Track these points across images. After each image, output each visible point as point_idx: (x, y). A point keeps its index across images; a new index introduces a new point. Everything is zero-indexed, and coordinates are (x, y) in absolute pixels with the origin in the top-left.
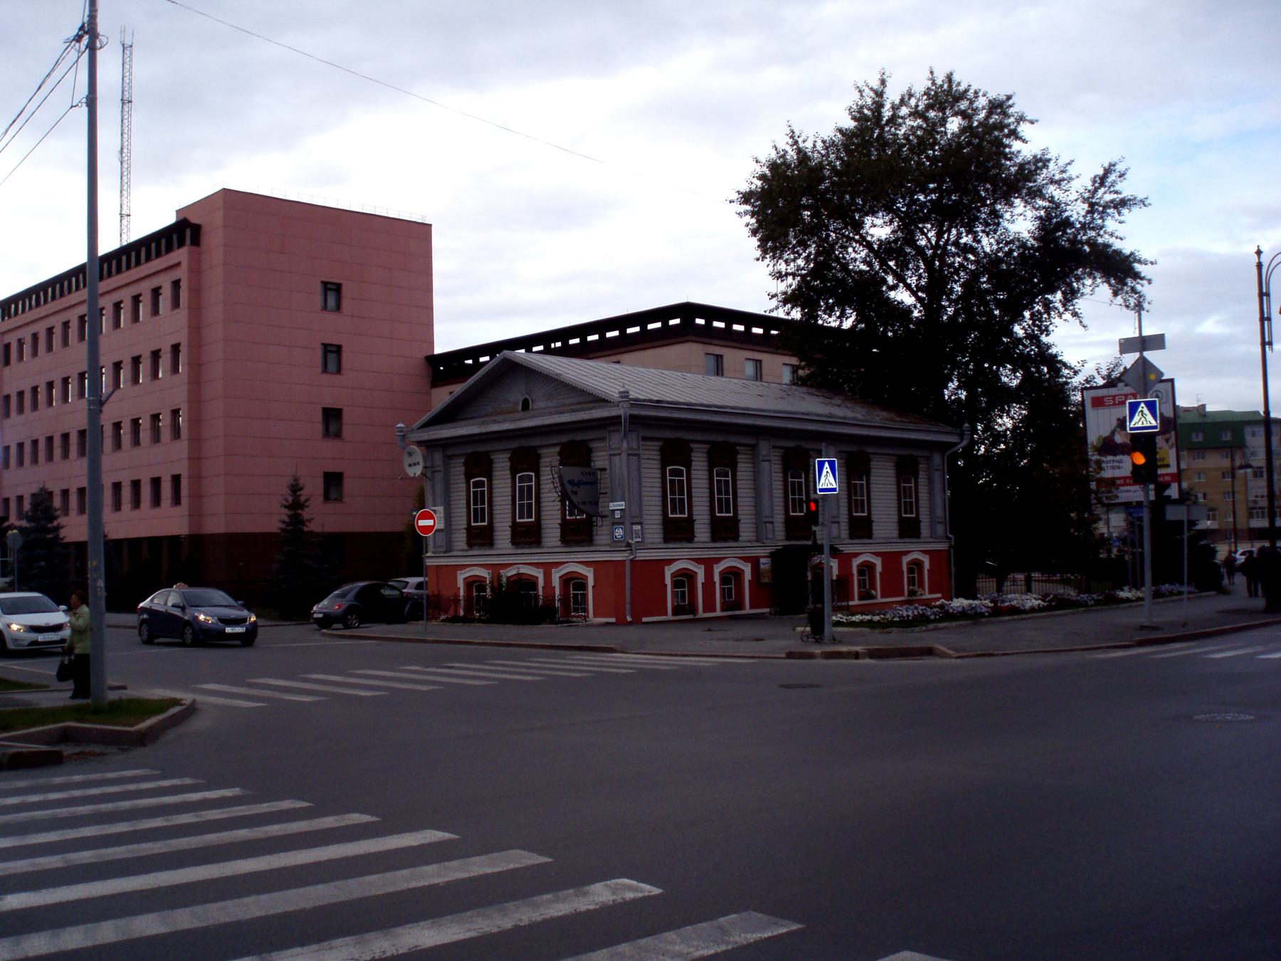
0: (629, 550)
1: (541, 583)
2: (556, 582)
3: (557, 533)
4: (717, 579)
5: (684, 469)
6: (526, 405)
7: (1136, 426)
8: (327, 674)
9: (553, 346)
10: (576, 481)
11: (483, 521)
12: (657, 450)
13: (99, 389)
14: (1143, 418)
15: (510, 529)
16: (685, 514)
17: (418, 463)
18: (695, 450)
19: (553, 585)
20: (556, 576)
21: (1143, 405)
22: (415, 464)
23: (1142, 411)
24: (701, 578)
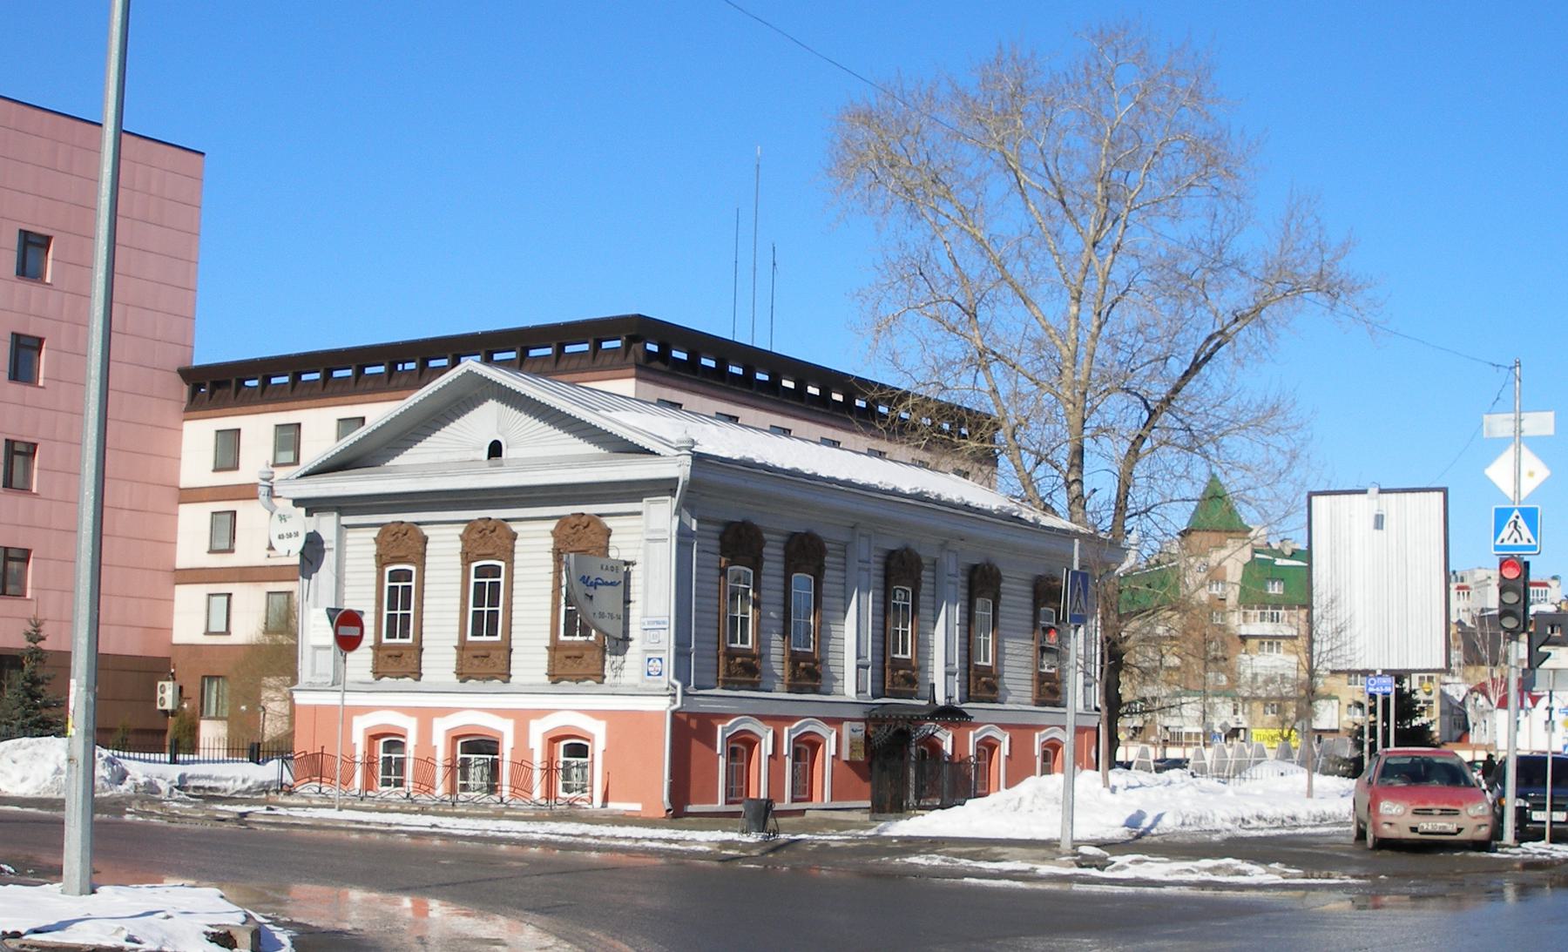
0: (671, 695)
1: (411, 742)
2: (440, 741)
3: (451, 658)
4: (786, 749)
5: (751, 571)
6: (495, 450)
7: (1506, 543)
8: (1479, 851)
9: (400, 367)
10: (592, 579)
11: (404, 635)
12: (715, 539)
13: (340, 366)
14: (1516, 533)
15: (455, 651)
16: (566, 634)
17: (297, 534)
18: (769, 543)
19: (434, 744)
20: (537, 733)
21: (1516, 513)
22: (290, 536)
23: (1516, 523)
24: (766, 746)
